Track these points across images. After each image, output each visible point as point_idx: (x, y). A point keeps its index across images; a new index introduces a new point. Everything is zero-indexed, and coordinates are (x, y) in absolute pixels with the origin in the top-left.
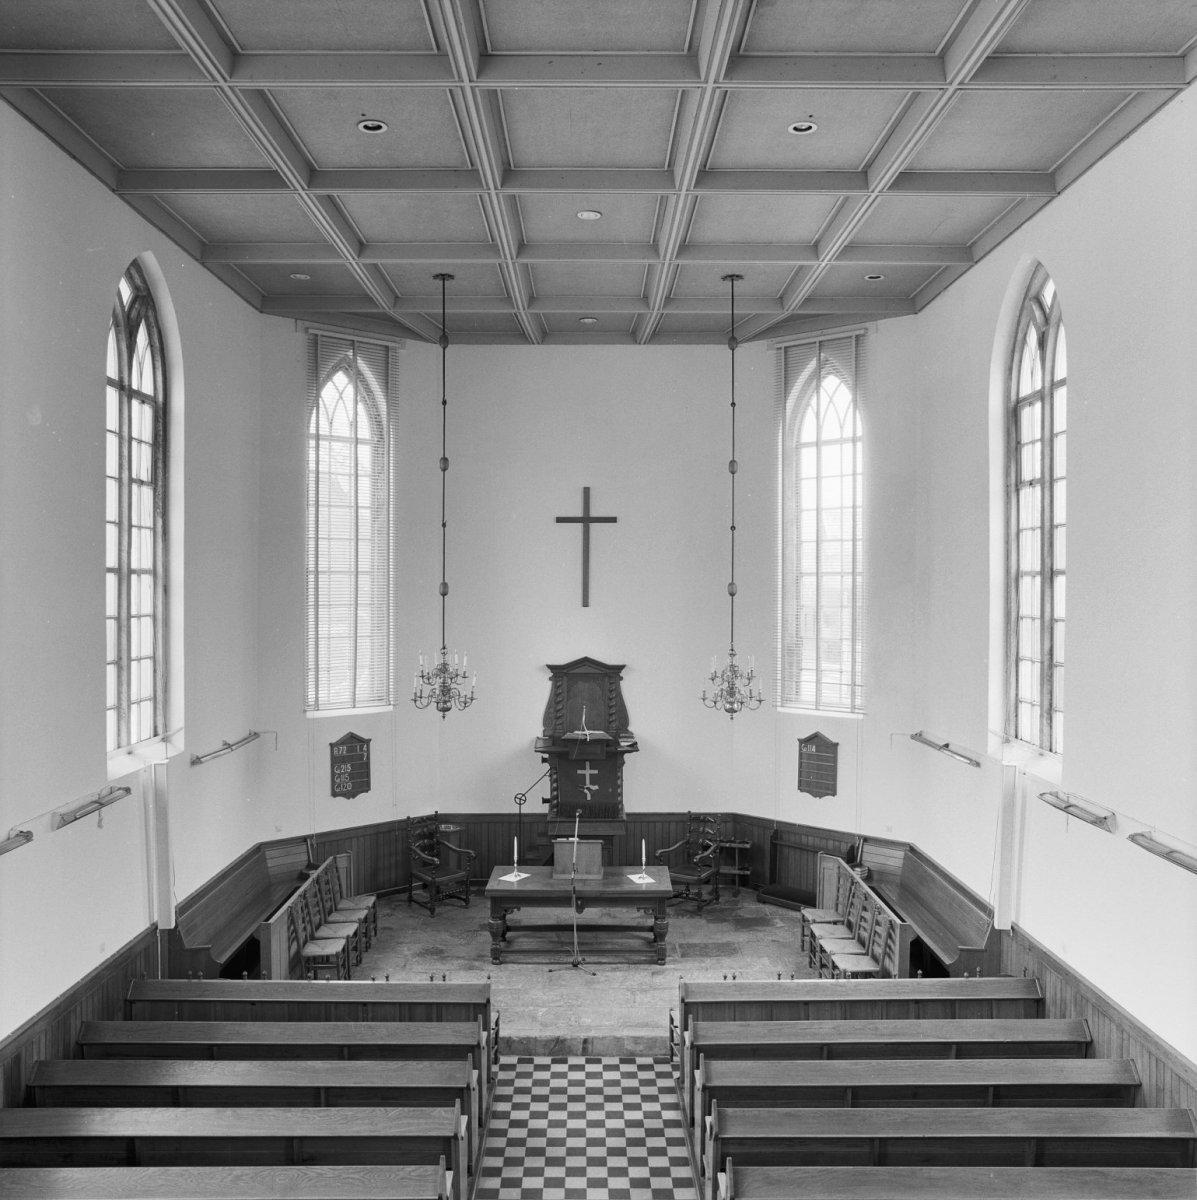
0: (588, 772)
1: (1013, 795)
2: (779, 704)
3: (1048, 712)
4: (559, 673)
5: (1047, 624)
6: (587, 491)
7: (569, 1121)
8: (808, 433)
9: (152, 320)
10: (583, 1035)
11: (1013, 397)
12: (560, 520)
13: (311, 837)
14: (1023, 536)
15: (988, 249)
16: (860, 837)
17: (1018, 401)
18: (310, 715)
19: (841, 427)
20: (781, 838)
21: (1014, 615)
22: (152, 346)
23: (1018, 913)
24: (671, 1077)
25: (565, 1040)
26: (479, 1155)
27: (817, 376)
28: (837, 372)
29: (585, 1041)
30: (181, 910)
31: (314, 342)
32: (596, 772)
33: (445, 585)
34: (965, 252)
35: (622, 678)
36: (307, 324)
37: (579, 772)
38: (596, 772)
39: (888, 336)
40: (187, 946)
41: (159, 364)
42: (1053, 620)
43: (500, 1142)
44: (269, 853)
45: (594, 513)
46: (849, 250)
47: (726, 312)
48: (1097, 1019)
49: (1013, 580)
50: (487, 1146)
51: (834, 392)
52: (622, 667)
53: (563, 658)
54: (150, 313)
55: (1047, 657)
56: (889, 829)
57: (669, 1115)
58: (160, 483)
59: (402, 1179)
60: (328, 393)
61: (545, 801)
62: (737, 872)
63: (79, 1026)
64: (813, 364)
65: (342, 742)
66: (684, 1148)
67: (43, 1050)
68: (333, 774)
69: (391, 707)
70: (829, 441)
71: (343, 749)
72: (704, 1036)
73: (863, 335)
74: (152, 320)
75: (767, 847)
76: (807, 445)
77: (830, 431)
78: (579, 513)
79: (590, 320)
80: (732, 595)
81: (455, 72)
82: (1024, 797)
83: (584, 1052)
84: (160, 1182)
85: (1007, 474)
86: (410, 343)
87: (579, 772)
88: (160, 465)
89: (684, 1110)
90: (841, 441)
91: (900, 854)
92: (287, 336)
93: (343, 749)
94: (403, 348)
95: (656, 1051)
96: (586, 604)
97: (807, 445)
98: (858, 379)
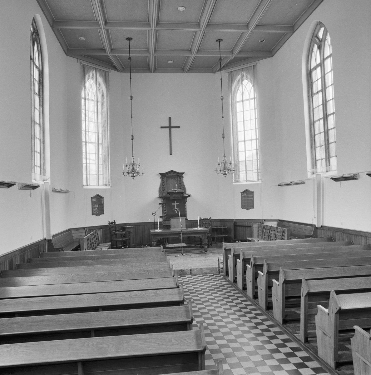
0: (176, 204)
1: (320, 184)
2: (234, 182)
3: (328, 158)
4: (163, 175)
5: (326, 132)
6: (170, 118)
8: (239, 97)
9: (38, 41)
10: (190, 269)
11: (309, 69)
12: (162, 127)
13: (86, 228)
14: (315, 110)
15: (299, 25)
16: (263, 220)
17: (311, 70)
18: (85, 187)
19: (249, 95)
20: (236, 224)
21: (313, 135)
22: (38, 51)
23: (323, 222)
24: (197, 322)
25: (184, 270)
27: (242, 79)
28: (247, 78)
29: (191, 270)
30: (53, 236)
31: (84, 66)
32: (178, 204)
33: (133, 136)
35: (183, 177)
36: (81, 61)
37: (173, 204)
38: (178, 204)
39: (263, 65)
40: (55, 248)
41: (40, 57)
44: (73, 232)
45: (172, 125)
46: (258, 26)
47: (217, 56)
48: (356, 239)
49: (312, 124)
51: (247, 85)
52: (183, 173)
53: (164, 171)
54: (38, 39)
55: (327, 142)
56: (272, 216)
58: (41, 96)
59: (159, 272)
60: (87, 84)
61: (160, 217)
62: (223, 236)
63: (27, 259)
64: (240, 76)
65: (95, 197)
67: (18, 261)
68: (92, 208)
69: (110, 187)
70: (245, 98)
71: (95, 200)
72: (237, 252)
73: (255, 65)
74: (38, 41)
75: (232, 228)
76: (239, 102)
77: (246, 97)
78: (168, 125)
79: (171, 62)
80: (224, 138)
82: (323, 185)
83: (191, 274)
84: (76, 278)
85: (308, 92)
86: (113, 71)
87: (173, 204)
88: (41, 90)
90: (250, 99)
91: (276, 223)
92: (75, 64)
93: (95, 200)
94: (111, 72)
95: (214, 272)
96: (171, 154)
97: (239, 102)
98: (255, 80)
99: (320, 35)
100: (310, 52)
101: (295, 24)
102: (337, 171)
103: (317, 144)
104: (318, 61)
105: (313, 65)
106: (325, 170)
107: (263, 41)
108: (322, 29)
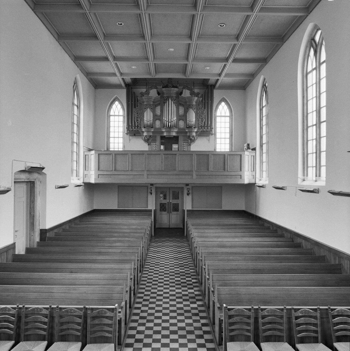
7: (162, 339)
26: (124, 338)
34: (253, 76)
38: (163, 141)
42: (263, 144)
43: (133, 332)
50: (133, 312)
57: (196, 293)
66: (209, 327)
81: (141, 9)
89: (202, 291)
99: (317, 38)
100: (306, 56)
101: (285, 36)
102: (325, 183)
103: (310, 164)
104: (314, 66)
105: (310, 69)
106: (314, 179)
107: (122, 24)
108: (319, 32)
